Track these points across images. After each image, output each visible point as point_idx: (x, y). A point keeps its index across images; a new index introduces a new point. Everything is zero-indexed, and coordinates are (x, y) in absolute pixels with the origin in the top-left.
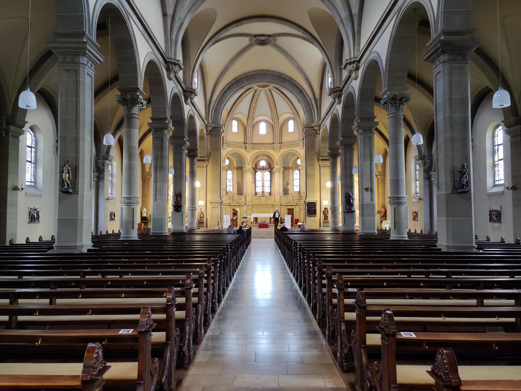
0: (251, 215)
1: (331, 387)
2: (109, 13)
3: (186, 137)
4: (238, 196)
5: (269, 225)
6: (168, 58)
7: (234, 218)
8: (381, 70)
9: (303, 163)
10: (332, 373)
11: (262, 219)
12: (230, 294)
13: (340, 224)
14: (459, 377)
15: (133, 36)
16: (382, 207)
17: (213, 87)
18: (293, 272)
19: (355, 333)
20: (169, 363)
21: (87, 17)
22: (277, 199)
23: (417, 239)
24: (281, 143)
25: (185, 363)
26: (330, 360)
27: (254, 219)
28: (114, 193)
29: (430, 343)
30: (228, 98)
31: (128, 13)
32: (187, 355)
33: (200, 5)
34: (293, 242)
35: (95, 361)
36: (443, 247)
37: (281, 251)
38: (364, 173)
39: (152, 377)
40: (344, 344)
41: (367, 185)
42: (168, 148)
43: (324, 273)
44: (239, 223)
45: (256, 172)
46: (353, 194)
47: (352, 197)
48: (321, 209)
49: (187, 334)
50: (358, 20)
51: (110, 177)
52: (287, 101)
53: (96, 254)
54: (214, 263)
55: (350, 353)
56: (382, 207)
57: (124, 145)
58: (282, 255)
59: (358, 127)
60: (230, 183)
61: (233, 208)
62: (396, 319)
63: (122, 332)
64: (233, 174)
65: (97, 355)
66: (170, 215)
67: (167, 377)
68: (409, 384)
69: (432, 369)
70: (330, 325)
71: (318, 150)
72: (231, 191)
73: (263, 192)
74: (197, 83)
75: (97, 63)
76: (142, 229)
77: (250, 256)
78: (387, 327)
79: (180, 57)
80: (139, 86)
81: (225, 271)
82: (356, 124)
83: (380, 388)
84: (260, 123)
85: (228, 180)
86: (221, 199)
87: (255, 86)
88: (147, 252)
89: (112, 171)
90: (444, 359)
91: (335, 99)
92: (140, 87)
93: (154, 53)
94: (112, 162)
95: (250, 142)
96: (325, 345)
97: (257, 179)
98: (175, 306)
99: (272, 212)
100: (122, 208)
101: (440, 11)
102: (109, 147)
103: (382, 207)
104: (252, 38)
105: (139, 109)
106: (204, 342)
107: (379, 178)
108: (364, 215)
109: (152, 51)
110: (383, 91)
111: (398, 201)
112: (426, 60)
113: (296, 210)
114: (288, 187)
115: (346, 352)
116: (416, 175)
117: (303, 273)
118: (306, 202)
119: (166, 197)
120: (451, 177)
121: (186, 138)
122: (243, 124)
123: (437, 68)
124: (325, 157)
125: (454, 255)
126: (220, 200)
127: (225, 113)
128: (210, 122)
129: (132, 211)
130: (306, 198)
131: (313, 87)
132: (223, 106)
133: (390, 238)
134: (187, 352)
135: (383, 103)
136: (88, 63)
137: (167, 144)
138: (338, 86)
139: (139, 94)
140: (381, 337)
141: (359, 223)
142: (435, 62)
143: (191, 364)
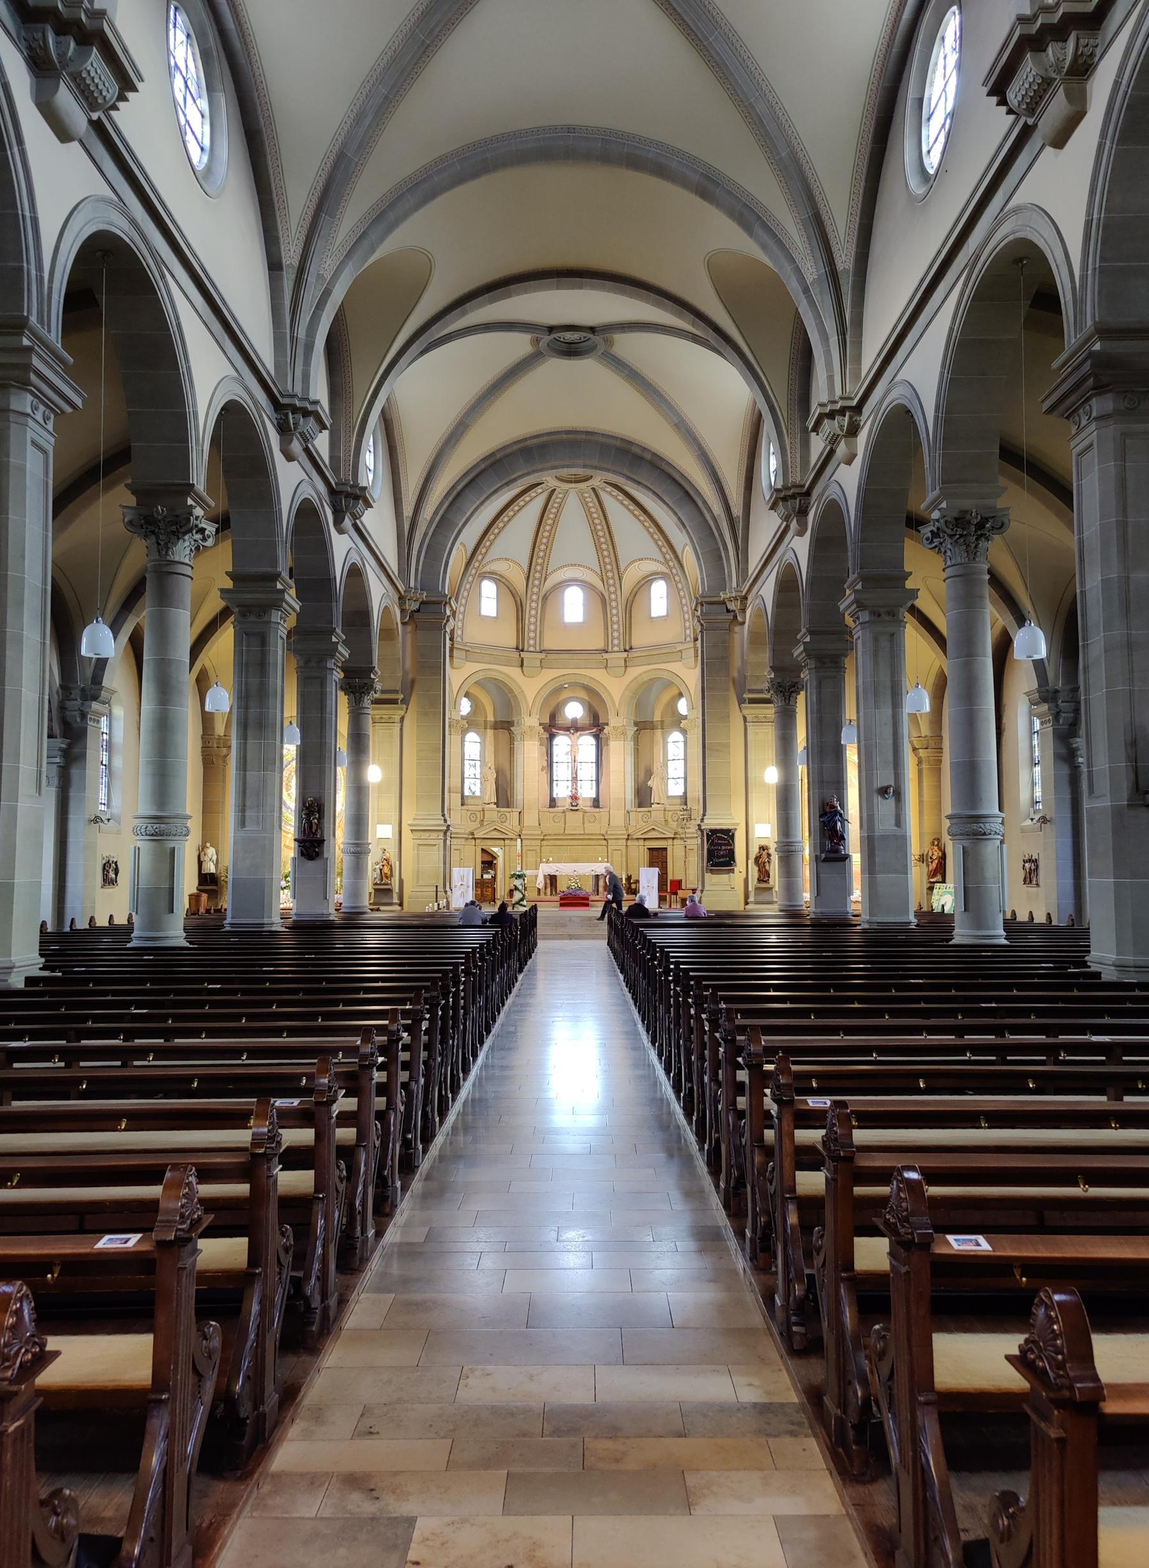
0: (537, 868)
1: (754, 1401)
2: (104, 259)
3: (339, 631)
4: (498, 809)
5: (592, 898)
6: (282, 396)
7: (486, 876)
8: (923, 435)
9: (695, 711)
10: (759, 1357)
11: (570, 880)
12: (462, 1114)
13: (807, 896)
14: (1096, 1375)
15: (175, 328)
16: (933, 842)
17: (422, 480)
18: (657, 1044)
19: (822, 1237)
20: (257, 1335)
21: (33, 272)
22: (618, 818)
23: (1034, 941)
24: (628, 648)
25: (312, 1331)
26: (756, 1317)
27: (545, 880)
28: (116, 801)
29: (1032, 1267)
30: (468, 514)
31: (160, 262)
32: (317, 1308)
33: (381, 240)
34: (658, 952)
35: (9, 1337)
36: (1106, 967)
37: (625, 978)
38: (874, 741)
39: (200, 1381)
40: (792, 1270)
41: (884, 778)
42: (283, 665)
43: (739, 1051)
44: (501, 892)
45: (552, 737)
46: (842, 806)
47: (841, 815)
48: (750, 849)
49: (319, 1243)
50: (853, 288)
51: (104, 753)
52: (646, 524)
53: (52, 994)
54: (410, 1022)
55: (811, 1297)
56: (933, 842)
57: (145, 658)
58: (627, 990)
59: (855, 606)
60: (472, 769)
61: (483, 847)
62: (934, 1191)
63: (107, 1243)
64: (483, 744)
65: (15, 1319)
66: (288, 868)
67: (249, 1377)
68: (973, 1391)
69: (1021, 1351)
70: (758, 1209)
71: (739, 672)
72: (478, 794)
73: (574, 798)
74: (372, 467)
75: (63, 412)
76: (202, 910)
77: (532, 995)
78: (906, 1220)
79: (320, 391)
80: (194, 480)
81: (447, 1043)
82: (850, 595)
83: (890, 1404)
84: (565, 590)
85: (466, 763)
86: (445, 821)
87: (550, 480)
88: (210, 986)
89: (110, 734)
90: (1051, 1321)
91: (787, 519)
92: (195, 483)
93: (240, 380)
94: (109, 706)
95: (534, 646)
96: (741, 1271)
97: (555, 759)
98: (277, 1159)
99: (600, 859)
100: (137, 850)
101: (1090, 267)
102: (102, 663)
103: (933, 844)
104: (539, 336)
105: (193, 548)
106: (375, 1264)
107: (921, 755)
108: (877, 868)
109: (235, 374)
110: (927, 499)
111: (974, 826)
112: (1050, 410)
113: (675, 853)
114: (649, 783)
115: (802, 1293)
116: (1032, 748)
117: (685, 1049)
118: (703, 828)
119: (276, 815)
120: (1129, 758)
121: (339, 636)
122: (514, 591)
123: (1083, 435)
124: (761, 692)
125: (1137, 993)
126: (442, 822)
127: (457, 558)
128: (412, 584)
129: (168, 861)
130: (704, 815)
131: (724, 484)
132: (452, 538)
133: (951, 940)
134: (318, 1297)
135: (929, 535)
136: (35, 412)
137: (280, 652)
138: (798, 480)
139: (194, 504)
140: (888, 1250)
141: (862, 891)
142: (1077, 418)
143: (329, 1333)
